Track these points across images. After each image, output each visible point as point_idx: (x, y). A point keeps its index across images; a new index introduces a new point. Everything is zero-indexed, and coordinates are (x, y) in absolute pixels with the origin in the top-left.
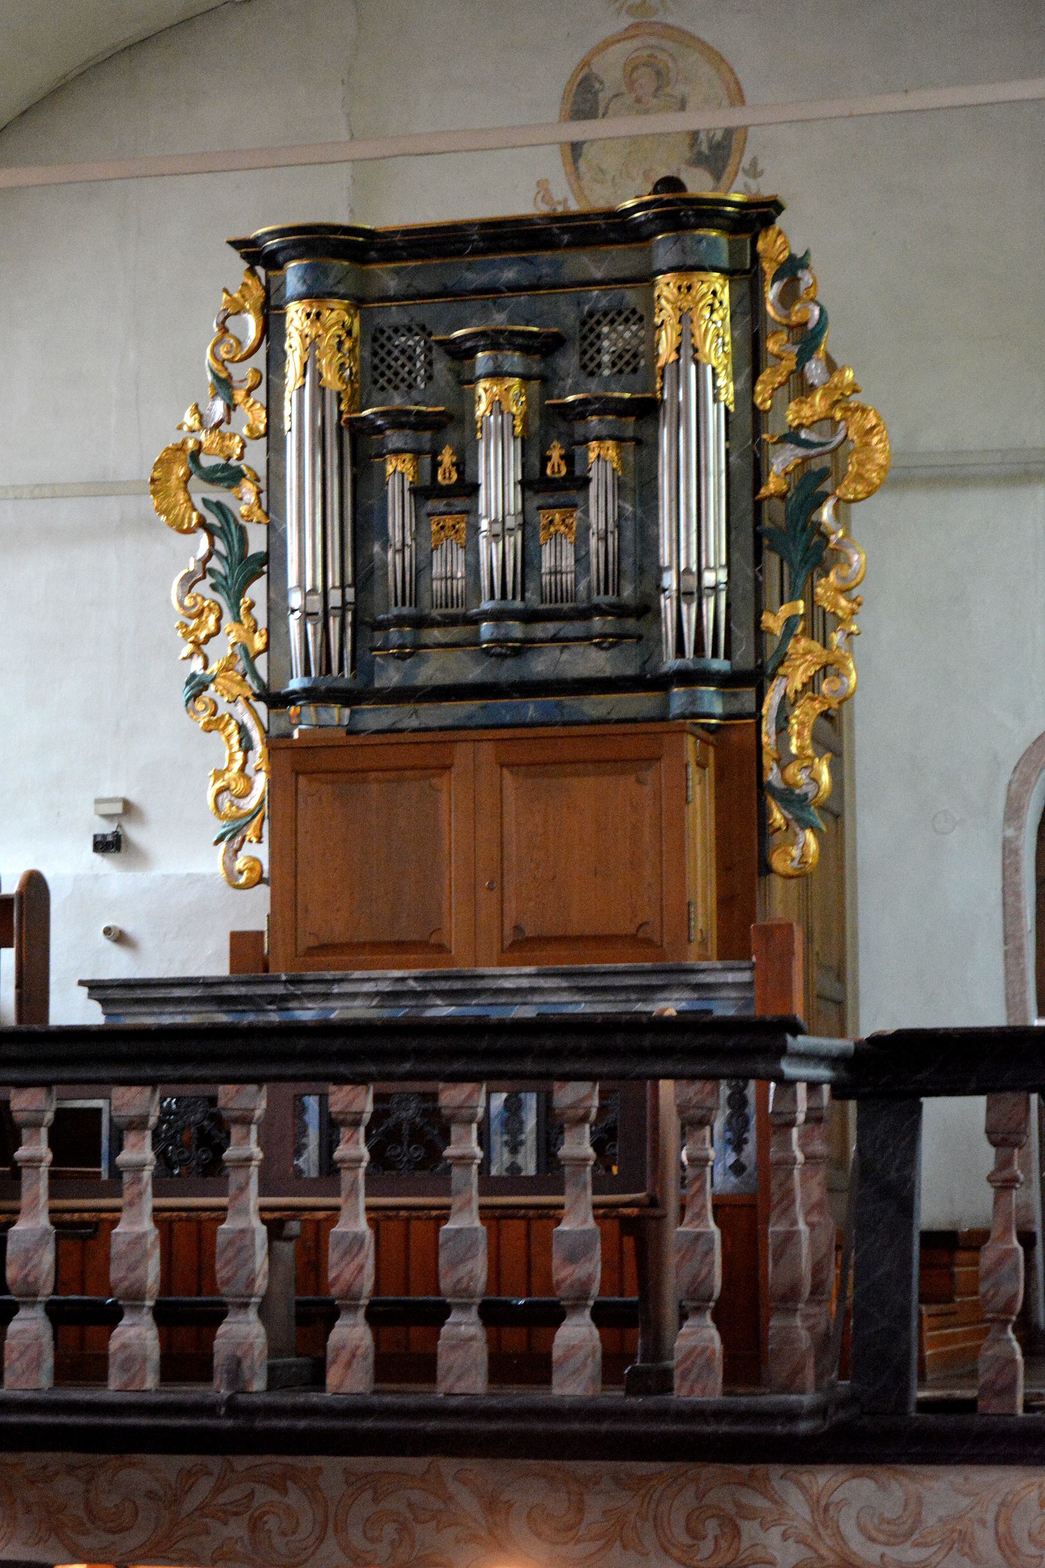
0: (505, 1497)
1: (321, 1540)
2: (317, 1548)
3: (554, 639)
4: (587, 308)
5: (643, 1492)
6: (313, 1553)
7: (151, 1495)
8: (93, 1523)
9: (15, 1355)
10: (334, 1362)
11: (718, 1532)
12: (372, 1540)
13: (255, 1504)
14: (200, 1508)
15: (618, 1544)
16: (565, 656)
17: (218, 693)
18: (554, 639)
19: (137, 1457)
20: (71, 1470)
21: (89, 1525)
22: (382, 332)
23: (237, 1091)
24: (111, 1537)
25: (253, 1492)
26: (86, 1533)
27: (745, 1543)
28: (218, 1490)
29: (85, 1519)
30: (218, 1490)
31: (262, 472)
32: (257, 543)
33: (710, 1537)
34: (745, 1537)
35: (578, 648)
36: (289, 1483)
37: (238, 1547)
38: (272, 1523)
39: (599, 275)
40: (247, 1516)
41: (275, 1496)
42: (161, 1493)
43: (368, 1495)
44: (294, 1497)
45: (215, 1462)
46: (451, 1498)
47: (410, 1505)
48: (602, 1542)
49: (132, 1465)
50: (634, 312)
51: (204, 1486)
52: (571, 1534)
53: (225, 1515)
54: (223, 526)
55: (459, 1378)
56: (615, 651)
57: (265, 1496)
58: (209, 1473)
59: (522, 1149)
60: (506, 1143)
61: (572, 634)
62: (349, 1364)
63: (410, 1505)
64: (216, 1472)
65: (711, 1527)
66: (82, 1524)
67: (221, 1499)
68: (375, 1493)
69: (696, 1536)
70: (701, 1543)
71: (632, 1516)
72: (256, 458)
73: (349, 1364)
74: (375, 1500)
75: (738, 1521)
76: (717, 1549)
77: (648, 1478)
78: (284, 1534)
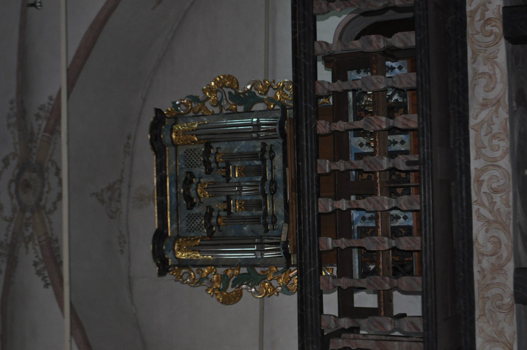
0: (481, 101)
1: (499, 167)
2: (502, 168)
3: (272, 171)
4: (183, 166)
5: (477, 53)
6: (504, 169)
7: (487, 231)
8: (498, 253)
9: (409, 246)
10: (407, 125)
11: (489, 26)
12: (499, 148)
13: (488, 191)
14: (491, 212)
15: (495, 60)
16: (277, 168)
17: (190, 167)
18: (272, 171)
19: (474, 238)
20: (480, 262)
21: (499, 254)
22: (187, 229)
23: (320, 166)
24: (503, 246)
25: (484, 192)
26: (501, 255)
27: (493, 16)
28: (484, 206)
29: (496, 256)
30: (484, 206)
31: (225, 269)
32: (244, 270)
33: (491, 28)
34: (491, 17)
35: (274, 163)
36: (481, 179)
37: (504, 197)
38: (494, 185)
39: (174, 163)
40: (492, 194)
41: (485, 185)
42: (486, 227)
43: (483, 151)
44: (485, 177)
45: (475, 207)
46: (483, 120)
47: (486, 135)
48: (495, 66)
49: (476, 239)
50: (185, 152)
51: (483, 211)
52: (493, 76)
53: (493, 203)
54: (240, 280)
55: (411, 79)
56: (275, 152)
57: (485, 188)
58: (479, 209)
59: (396, 140)
60: (394, 145)
61: (270, 165)
62: (408, 120)
63: (486, 135)
64: (478, 207)
65: (488, 28)
66: (498, 257)
67: (487, 203)
68: (482, 148)
69: (491, 33)
70: (494, 31)
71: (485, 55)
72: (221, 270)
73: (408, 120)
74: (485, 148)
75: (486, 18)
76: (495, 26)
77: (473, 51)
78: (498, 181)
